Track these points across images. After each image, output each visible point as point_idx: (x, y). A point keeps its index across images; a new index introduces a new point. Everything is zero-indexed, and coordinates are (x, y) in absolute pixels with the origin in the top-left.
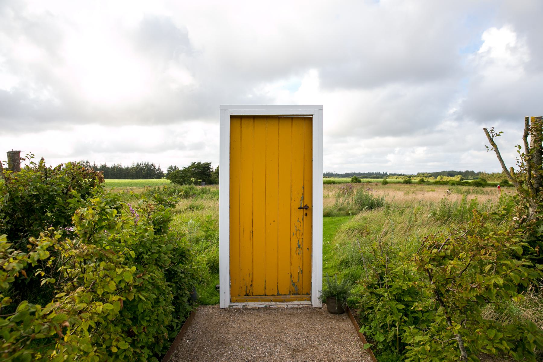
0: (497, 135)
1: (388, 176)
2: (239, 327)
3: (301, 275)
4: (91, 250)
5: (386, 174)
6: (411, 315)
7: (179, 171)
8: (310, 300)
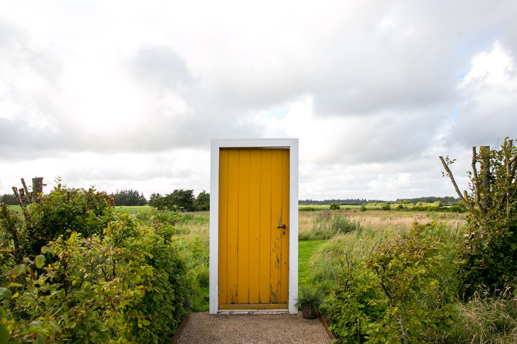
0: (451, 163)
1: (367, 203)
2: (227, 328)
3: (279, 286)
4: (123, 252)
5: (366, 200)
6: (370, 314)
7: (162, 198)
8: (287, 308)
